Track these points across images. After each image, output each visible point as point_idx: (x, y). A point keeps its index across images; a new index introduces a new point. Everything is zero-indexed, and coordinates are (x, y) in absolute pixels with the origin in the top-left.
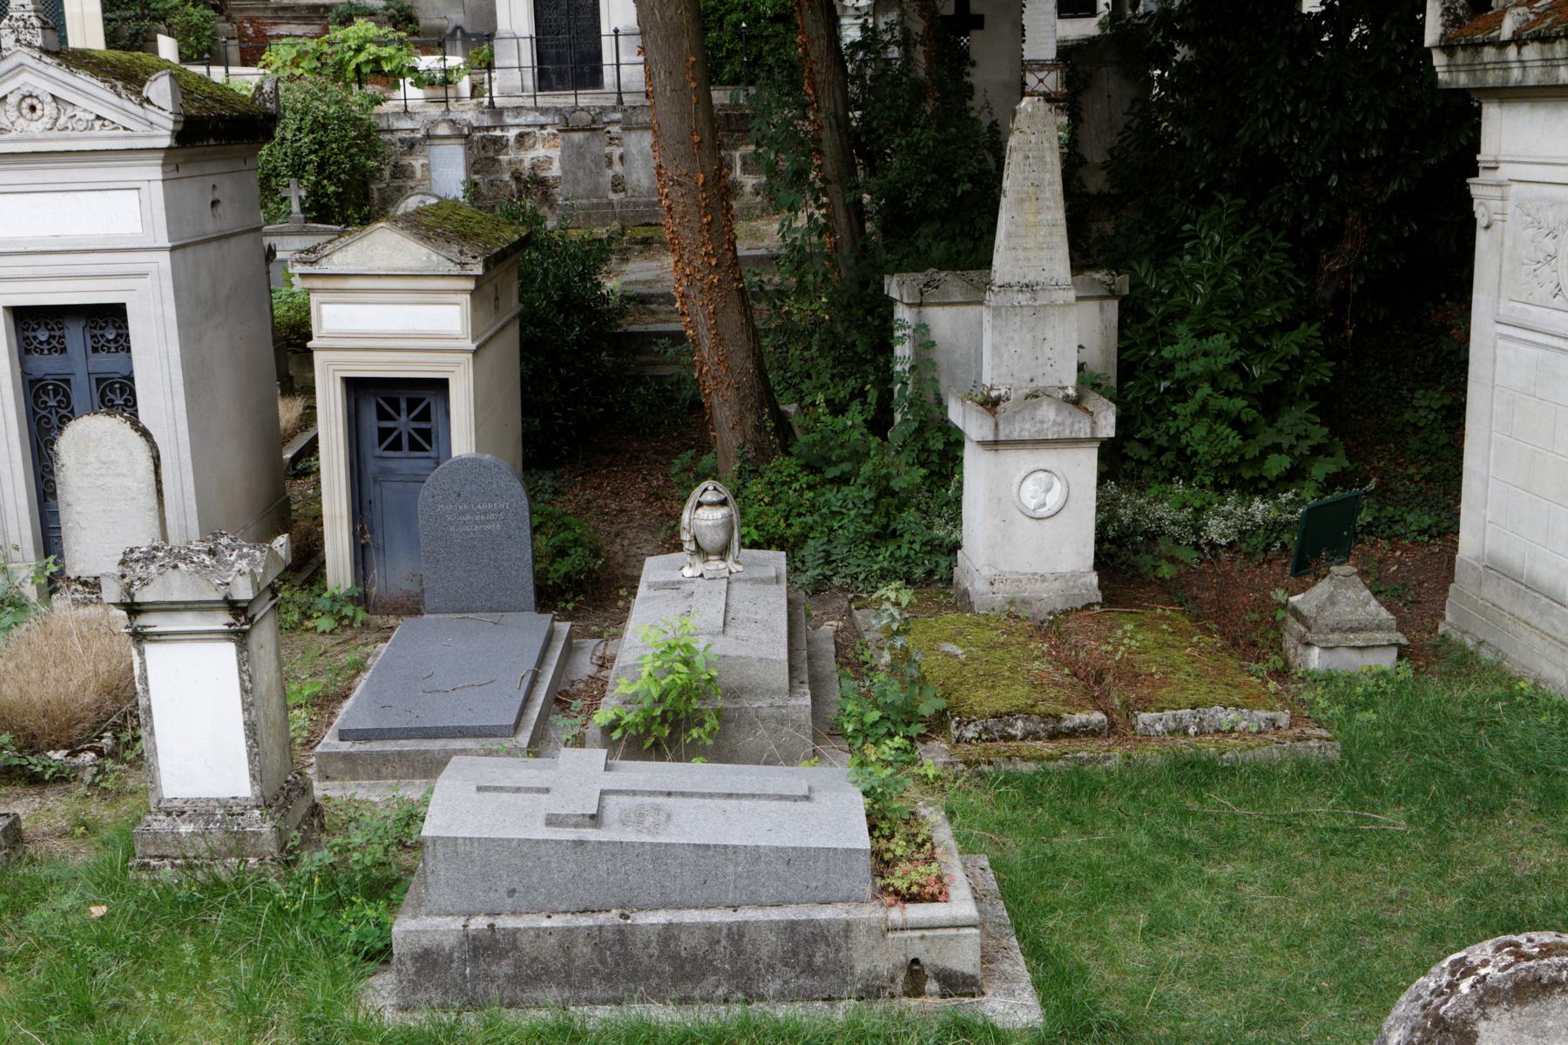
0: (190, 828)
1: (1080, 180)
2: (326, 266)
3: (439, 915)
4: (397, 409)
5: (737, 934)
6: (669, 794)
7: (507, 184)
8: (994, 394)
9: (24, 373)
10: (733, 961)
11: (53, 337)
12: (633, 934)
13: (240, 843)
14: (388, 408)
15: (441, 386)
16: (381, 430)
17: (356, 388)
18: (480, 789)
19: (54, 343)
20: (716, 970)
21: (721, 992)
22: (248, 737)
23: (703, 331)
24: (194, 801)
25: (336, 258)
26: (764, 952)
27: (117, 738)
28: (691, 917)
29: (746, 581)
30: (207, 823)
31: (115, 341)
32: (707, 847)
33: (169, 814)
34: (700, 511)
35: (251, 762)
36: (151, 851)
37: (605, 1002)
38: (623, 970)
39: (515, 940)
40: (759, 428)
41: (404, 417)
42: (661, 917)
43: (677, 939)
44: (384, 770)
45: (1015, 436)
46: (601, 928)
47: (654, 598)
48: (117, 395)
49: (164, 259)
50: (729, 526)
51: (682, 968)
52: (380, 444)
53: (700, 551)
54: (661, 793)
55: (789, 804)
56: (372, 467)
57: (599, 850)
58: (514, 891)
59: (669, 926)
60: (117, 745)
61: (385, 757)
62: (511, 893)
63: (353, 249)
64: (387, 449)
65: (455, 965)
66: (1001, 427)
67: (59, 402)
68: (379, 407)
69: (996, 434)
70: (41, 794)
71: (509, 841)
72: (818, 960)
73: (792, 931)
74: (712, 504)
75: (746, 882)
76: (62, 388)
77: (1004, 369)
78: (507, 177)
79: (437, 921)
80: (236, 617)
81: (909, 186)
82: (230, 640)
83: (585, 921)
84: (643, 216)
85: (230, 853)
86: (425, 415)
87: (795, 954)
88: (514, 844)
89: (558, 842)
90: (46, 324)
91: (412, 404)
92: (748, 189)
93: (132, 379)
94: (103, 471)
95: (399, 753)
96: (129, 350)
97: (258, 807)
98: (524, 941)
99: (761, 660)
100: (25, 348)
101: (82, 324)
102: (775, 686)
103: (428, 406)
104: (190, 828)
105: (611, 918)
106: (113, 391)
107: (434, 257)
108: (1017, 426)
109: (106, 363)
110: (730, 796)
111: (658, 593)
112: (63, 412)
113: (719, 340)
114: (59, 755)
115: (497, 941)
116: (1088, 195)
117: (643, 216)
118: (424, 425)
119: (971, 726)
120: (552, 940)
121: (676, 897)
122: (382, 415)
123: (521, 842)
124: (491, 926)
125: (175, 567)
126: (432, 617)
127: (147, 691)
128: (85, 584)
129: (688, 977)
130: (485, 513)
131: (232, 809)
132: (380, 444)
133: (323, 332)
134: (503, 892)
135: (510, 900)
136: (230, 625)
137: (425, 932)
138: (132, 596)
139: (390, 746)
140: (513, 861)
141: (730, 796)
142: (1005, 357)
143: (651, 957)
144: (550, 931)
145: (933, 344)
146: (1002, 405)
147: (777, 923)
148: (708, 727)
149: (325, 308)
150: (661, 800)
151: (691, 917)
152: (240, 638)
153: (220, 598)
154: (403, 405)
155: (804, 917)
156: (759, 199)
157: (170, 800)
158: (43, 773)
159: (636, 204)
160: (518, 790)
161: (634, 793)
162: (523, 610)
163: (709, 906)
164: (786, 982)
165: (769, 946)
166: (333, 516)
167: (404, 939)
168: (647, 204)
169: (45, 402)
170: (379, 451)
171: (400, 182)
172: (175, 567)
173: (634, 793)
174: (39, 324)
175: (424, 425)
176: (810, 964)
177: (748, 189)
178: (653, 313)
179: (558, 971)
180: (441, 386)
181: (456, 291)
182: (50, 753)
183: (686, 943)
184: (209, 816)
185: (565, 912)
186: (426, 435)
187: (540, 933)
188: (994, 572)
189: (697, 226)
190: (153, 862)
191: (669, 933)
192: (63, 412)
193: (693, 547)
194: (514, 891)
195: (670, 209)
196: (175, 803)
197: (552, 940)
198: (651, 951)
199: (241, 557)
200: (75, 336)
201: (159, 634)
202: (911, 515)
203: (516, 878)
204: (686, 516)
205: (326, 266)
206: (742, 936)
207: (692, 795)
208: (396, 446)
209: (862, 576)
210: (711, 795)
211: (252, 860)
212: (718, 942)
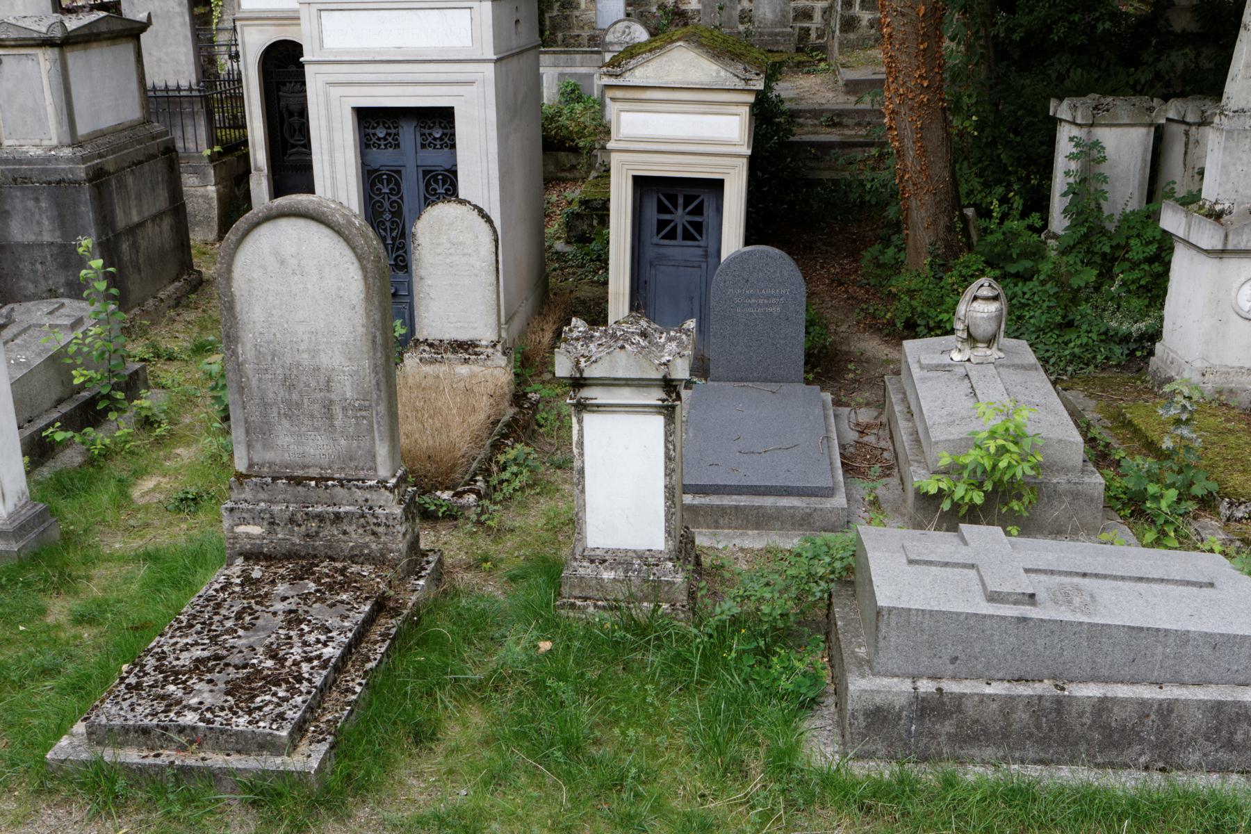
0: (612, 575)
1: (1167, 20)
2: (629, 79)
3: (886, 676)
4: (675, 203)
5: (1167, 710)
6: (1085, 575)
7: (653, 15)
8: (1218, 208)
9: (363, 164)
10: (1159, 733)
11: (389, 134)
12: (1070, 705)
13: (656, 589)
14: (667, 203)
15: (717, 186)
16: (659, 221)
17: (642, 184)
18: (911, 562)
19: (390, 139)
20: (1141, 741)
21: (1142, 760)
22: (667, 498)
23: (908, 143)
24: (614, 551)
25: (638, 72)
26: (1189, 728)
27: (487, 482)
28: (1122, 691)
29: (1008, 366)
30: (626, 571)
31: (441, 139)
32: (1141, 629)
33: (592, 562)
34: (975, 304)
35: (667, 520)
36: (577, 592)
37: (1036, 762)
38: (1055, 736)
39: (960, 704)
40: (950, 229)
41: (680, 211)
42: (1092, 691)
43: (1110, 711)
44: (721, 521)
45: (1242, 246)
46: (1040, 697)
47: (931, 379)
48: (443, 184)
49: (489, 69)
50: (999, 318)
51: (1111, 736)
52: (658, 233)
53: (971, 339)
54: (1077, 574)
55: (1195, 590)
56: (649, 253)
57: (1040, 627)
58: (957, 658)
59: (1104, 700)
60: (488, 487)
61: (723, 510)
62: (954, 660)
63: (653, 65)
64: (664, 238)
65: (902, 722)
66: (1230, 237)
67: (447, 190)
68: (659, 201)
69: (1225, 243)
70: (433, 528)
71: (958, 614)
72: (1239, 737)
73: (1218, 710)
74: (986, 299)
75: (1172, 662)
76: (393, 178)
77: (1230, 186)
78: (654, 9)
79: (886, 681)
80: (669, 394)
81: (1055, 22)
82: (660, 413)
83: (1022, 690)
84: (766, 44)
85: (646, 598)
86: (699, 210)
87: (1218, 730)
88: (962, 618)
89: (1003, 618)
90: (384, 123)
91: (688, 200)
92: (865, 23)
93: (455, 173)
94: (452, 251)
95: (736, 507)
96: (453, 146)
97: (670, 559)
98: (968, 706)
99: (1060, 441)
100: (366, 143)
101: (414, 124)
102: (1070, 464)
103: (702, 202)
104: (612, 575)
105: (1045, 688)
106: (436, 182)
107: (723, 73)
108: (1245, 238)
109: (433, 157)
110: (1140, 579)
111: (931, 374)
112: (394, 198)
113: (923, 152)
114: (446, 495)
115: (944, 704)
116: (1173, 33)
117: (766, 44)
118: (697, 219)
119: (1242, 507)
120: (994, 706)
121: (1105, 672)
122: (662, 209)
123: (968, 616)
124: (939, 690)
125: (622, 347)
126: (716, 384)
127: (582, 455)
128: (431, 345)
129: (1115, 745)
130: (768, 298)
131: (647, 559)
132: (658, 233)
133: (621, 136)
134: (946, 659)
135: (951, 667)
136: (663, 401)
137: (879, 692)
138: (581, 371)
139: (728, 501)
140: (960, 632)
141: (1140, 579)
142: (1233, 175)
143: (1083, 725)
144: (992, 698)
145: (1104, 159)
146: (1225, 217)
147: (1205, 702)
148: (1026, 500)
149: (624, 115)
150: (1077, 580)
151: (1122, 691)
152: (668, 411)
153: (660, 376)
154: (681, 201)
155: (1230, 699)
156: (873, 31)
157: (593, 550)
158: (436, 511)
159: (761, 34)
160: (946, 564)
161: (1052, 572)
162: (793, 382)
163: (1133, 682)
164: (1205, 755)
165: (1193, 722)
166: (617, 294)
167: (859, 697)
168: (770, 34)
169: (434, 189)
170: (656, 240)
171: (567, 12)
172: (622, 347)
173: (1052, 572)
174: (378, 123)
175: (697, 219)
176: (1230, 740)
177: (865, 23)
178: (802, 125)
179: (996, 733)
180: (717, 186)
181: (737, 104)
182: (438, 493)
183: (1118, 714)
184: (627, 566)
185: (1002, 680)
186: (698, 227)
187: (983, 698)
188: (1206, 364)
189: (913, 51)
190: (579, 603)
191: (1103, 705)
192: (394, 198)
193: (965, 336)
194: (957, 658)
195: (890, 36)
196: (598, 552)
197: (994, 706)
198: (1084, 720)
199: (670, 339)
200: (408, 133)
201: (598, 406)
202: (1085, 308)
203: (960, 648)
204: (962, 309)
205: (629, 79)
206: (1170, 711)
207: (1105, 577)
208: (671, 235)
209: (1052, 360)
210: (1123, 578)
211: (665, 606)
212: (1148, 716)
